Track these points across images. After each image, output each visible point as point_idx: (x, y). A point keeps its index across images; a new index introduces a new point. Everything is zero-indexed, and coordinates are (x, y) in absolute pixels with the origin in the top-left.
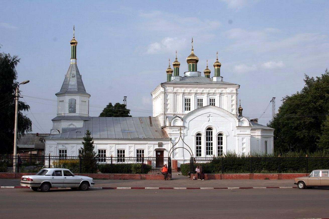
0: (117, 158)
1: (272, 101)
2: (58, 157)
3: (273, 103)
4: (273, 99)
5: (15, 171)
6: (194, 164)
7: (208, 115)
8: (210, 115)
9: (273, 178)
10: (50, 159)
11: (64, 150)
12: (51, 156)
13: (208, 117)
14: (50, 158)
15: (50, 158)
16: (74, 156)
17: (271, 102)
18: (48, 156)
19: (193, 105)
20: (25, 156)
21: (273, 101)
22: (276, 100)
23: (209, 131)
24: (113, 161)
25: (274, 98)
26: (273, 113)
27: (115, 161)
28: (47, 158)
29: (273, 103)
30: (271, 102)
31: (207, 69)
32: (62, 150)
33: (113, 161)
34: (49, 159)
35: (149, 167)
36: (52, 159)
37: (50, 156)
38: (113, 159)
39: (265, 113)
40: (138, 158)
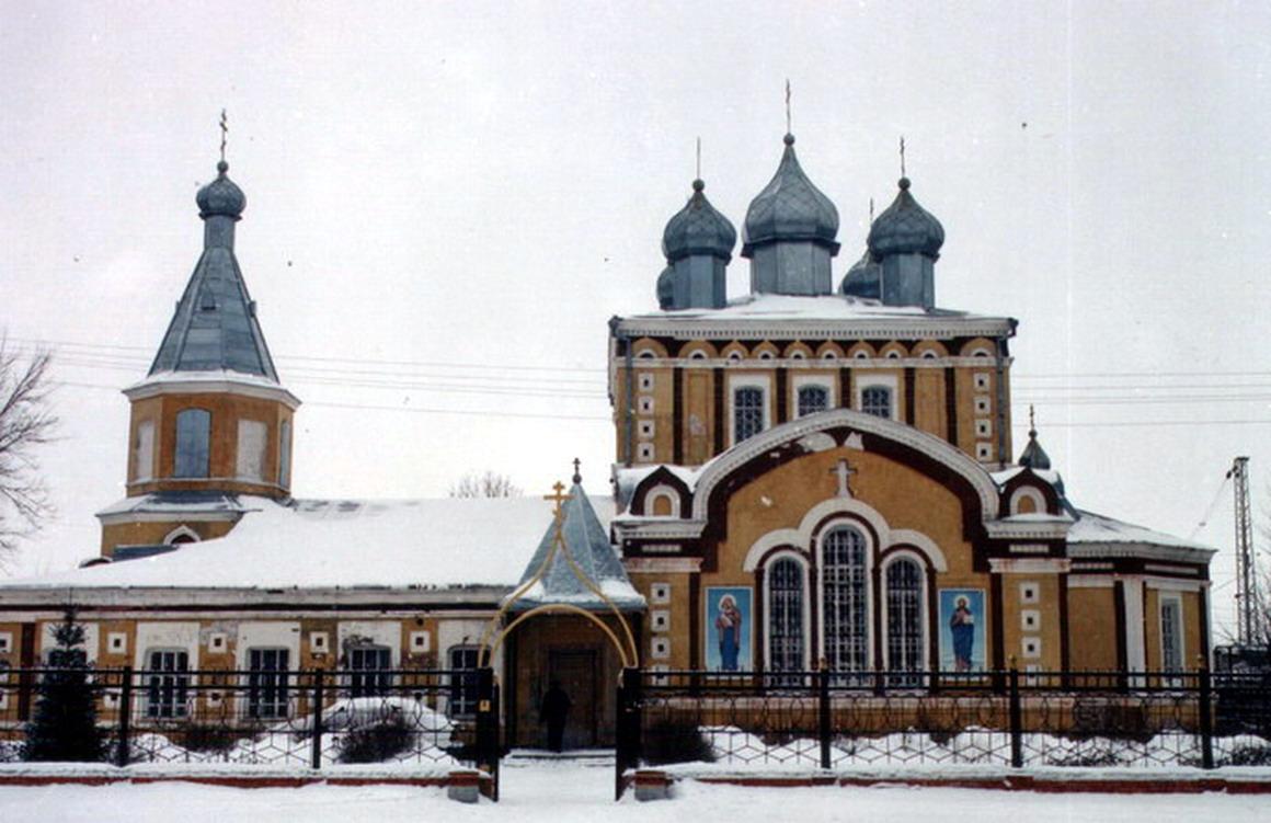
0: (149, 673)
1: (1233, 475)
2: (243, 673)
3: (1238, 481)
4: (1240, 467)
5: (1134, 708)
6: (244, 721)
9: (1235, 775)
11: (175, 652)
17: (1229, 475)
18: (118, 673)
19: (323, 370)
21: (1238, 471)
22: (1250, 467)
25: (1243, 460)
26: (1240, 525)
29: (1238, 481)
30: (1229, 475)
32: (163, 652)
33: (831, 693)
35: (405, 727)
39: (1206, 527)
40: (170, 676)
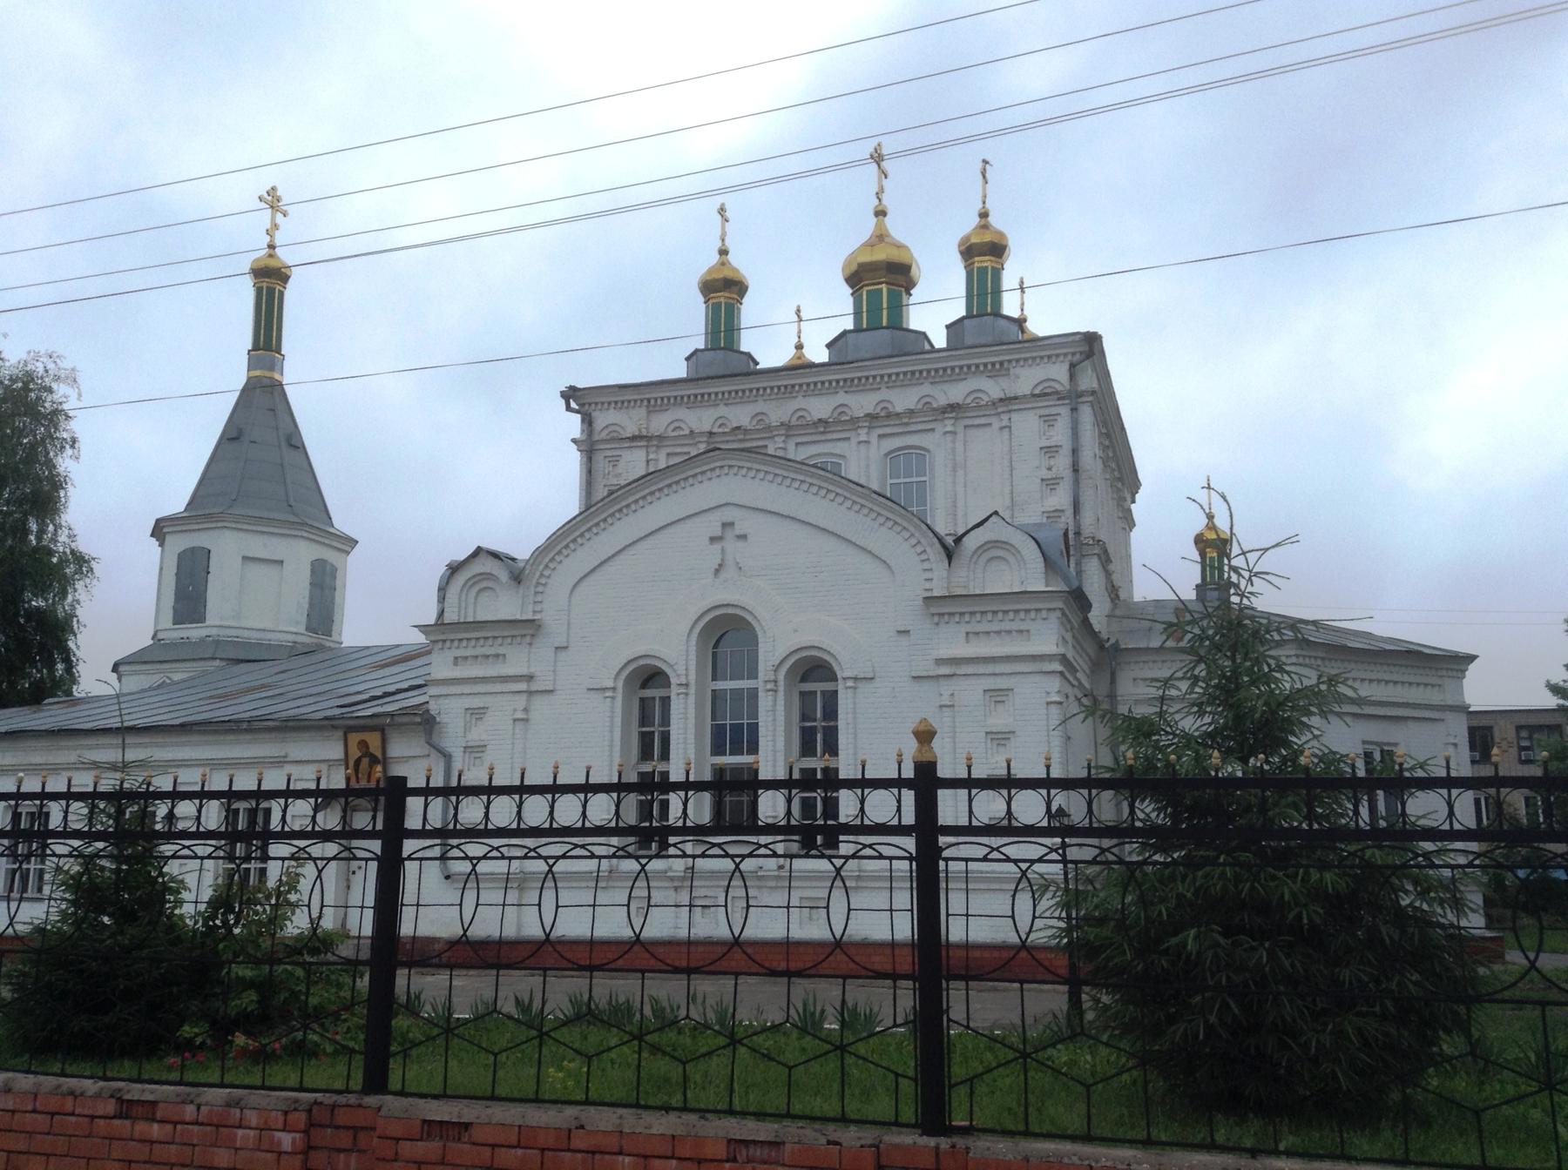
7: (712, 524)
8: (727, 525)
10: (927, 828)
12: (944, 771)
13: (713, 540)
14: (926, 807)
15: (926, 807)
16: (1020, 772)
18: (898, 783)
20: (444, 792)
23: (726, 636)
24: (409, 846)
27: (331, 849)
28: (881, 807)
31: (880, 237)
33: (409, 846)
34: (909, 843)
36: (567, 831)
37: (926, 782)
38: (951, 806)
